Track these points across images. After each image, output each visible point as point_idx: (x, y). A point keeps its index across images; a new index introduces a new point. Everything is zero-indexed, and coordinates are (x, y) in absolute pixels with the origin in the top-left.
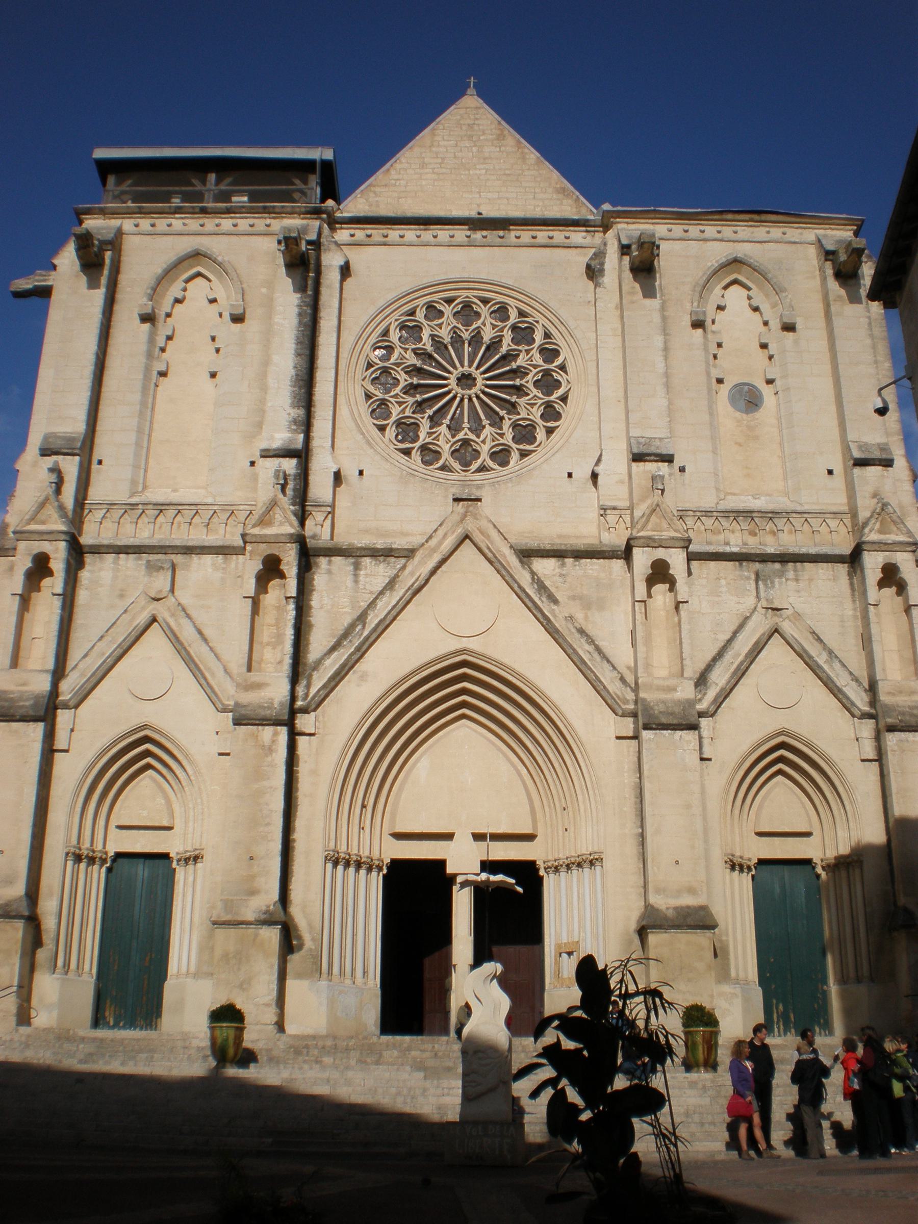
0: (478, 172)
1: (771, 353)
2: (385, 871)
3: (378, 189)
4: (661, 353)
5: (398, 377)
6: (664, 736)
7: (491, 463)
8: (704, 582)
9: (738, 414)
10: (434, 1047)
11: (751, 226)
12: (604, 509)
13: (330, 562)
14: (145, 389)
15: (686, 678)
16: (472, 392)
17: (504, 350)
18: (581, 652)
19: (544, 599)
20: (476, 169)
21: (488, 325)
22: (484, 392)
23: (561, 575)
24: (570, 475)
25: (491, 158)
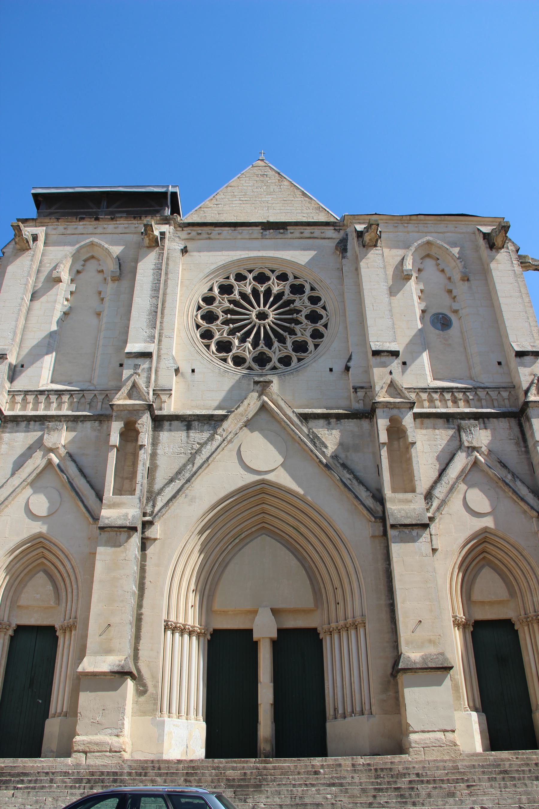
0: (267, 199)
2: (209, 637)
6: (406, 533)
12: (355, 389)
13: (170, 425)
17: (285, 298)
24: (331, 370)
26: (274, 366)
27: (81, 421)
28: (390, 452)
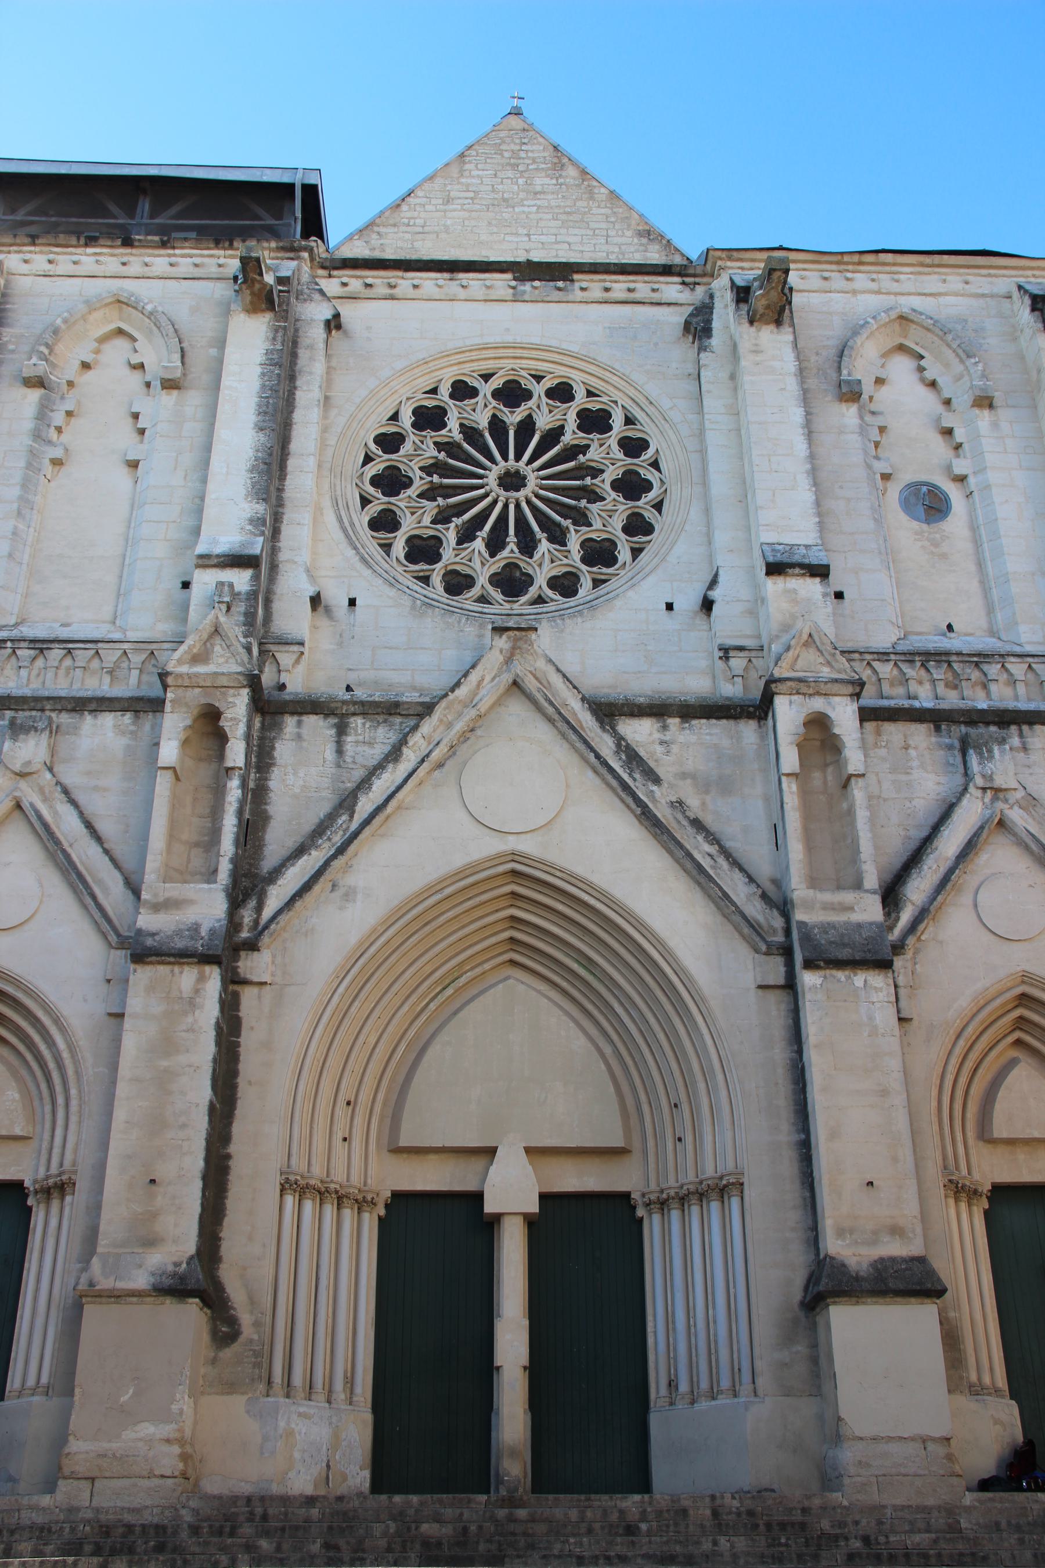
0: (526, 209)
1: (958, 440)
2: (382, 1212)
3: (382, 230)
4: (801, 431)
5: (411, 474)
6: (839, 981)
7: (550, 593)
8: (883, 752)
9: (915, 525)
10: (461, 1514)
11: (920, 273)
13: (299, 724)
14: (26, 484)
15: (867, 891)
16: (521, 494)
18: (698, 856)
19: (637, 776)
20: (523, 206)
21: (545, 409)
22: (537, 496)
23: (662, 743)
24: (670, 607)
25: (544, 193)
26: (540, 596)
27: (91, 711)
28: (805, 793)
